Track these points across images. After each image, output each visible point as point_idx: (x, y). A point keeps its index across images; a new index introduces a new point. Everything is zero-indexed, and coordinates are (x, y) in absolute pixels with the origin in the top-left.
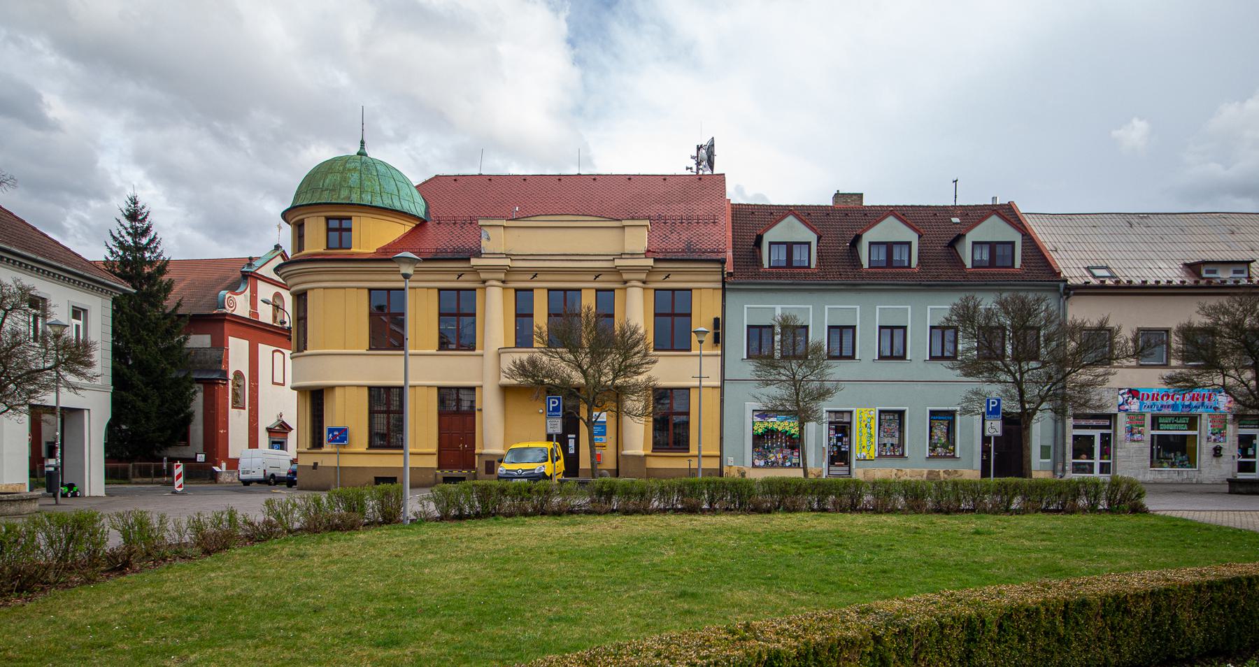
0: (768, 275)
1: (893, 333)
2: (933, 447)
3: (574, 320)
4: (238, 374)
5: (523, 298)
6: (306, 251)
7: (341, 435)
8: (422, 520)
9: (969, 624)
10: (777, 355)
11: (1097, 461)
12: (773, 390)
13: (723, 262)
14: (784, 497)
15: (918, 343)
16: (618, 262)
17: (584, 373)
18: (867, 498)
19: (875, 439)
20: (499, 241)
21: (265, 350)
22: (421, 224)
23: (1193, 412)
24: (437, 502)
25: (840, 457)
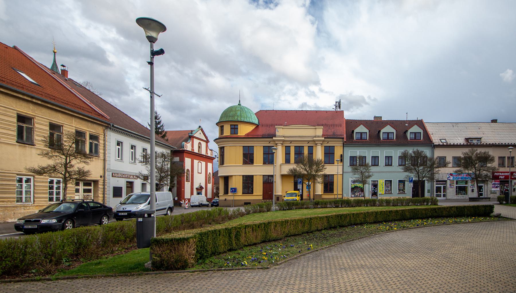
0: (356, 142)
1: (389, 159)
2: (399, 190)
3: (300, 154)
4: (188, 170)
5: (288, 148)
6: (224, 135)
7: (234, 190)
8: (276, 210)
9: (376, 212)
10: (358, 164)
11: (442, 194)
12: (356, 176)
13: (343, 138)
14: (358, 203)
15: (396, 161)
16: (314, 139)
17: (307, 172)
18: (377, 203)
19: (384, 189)
20: (281, 132)
21: (196, 162)
22: (257, 126)
23: (467, 180)
24: (278, 206)
25: (375, 194)
